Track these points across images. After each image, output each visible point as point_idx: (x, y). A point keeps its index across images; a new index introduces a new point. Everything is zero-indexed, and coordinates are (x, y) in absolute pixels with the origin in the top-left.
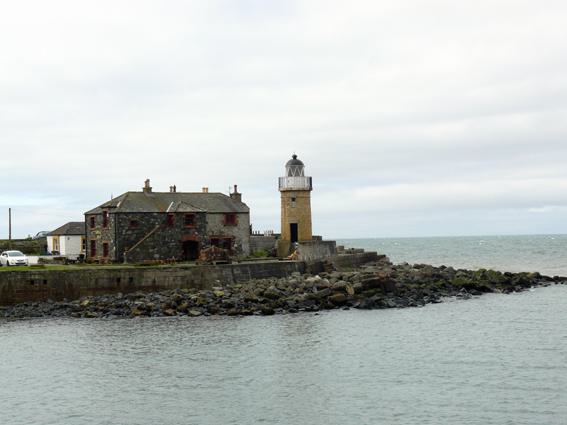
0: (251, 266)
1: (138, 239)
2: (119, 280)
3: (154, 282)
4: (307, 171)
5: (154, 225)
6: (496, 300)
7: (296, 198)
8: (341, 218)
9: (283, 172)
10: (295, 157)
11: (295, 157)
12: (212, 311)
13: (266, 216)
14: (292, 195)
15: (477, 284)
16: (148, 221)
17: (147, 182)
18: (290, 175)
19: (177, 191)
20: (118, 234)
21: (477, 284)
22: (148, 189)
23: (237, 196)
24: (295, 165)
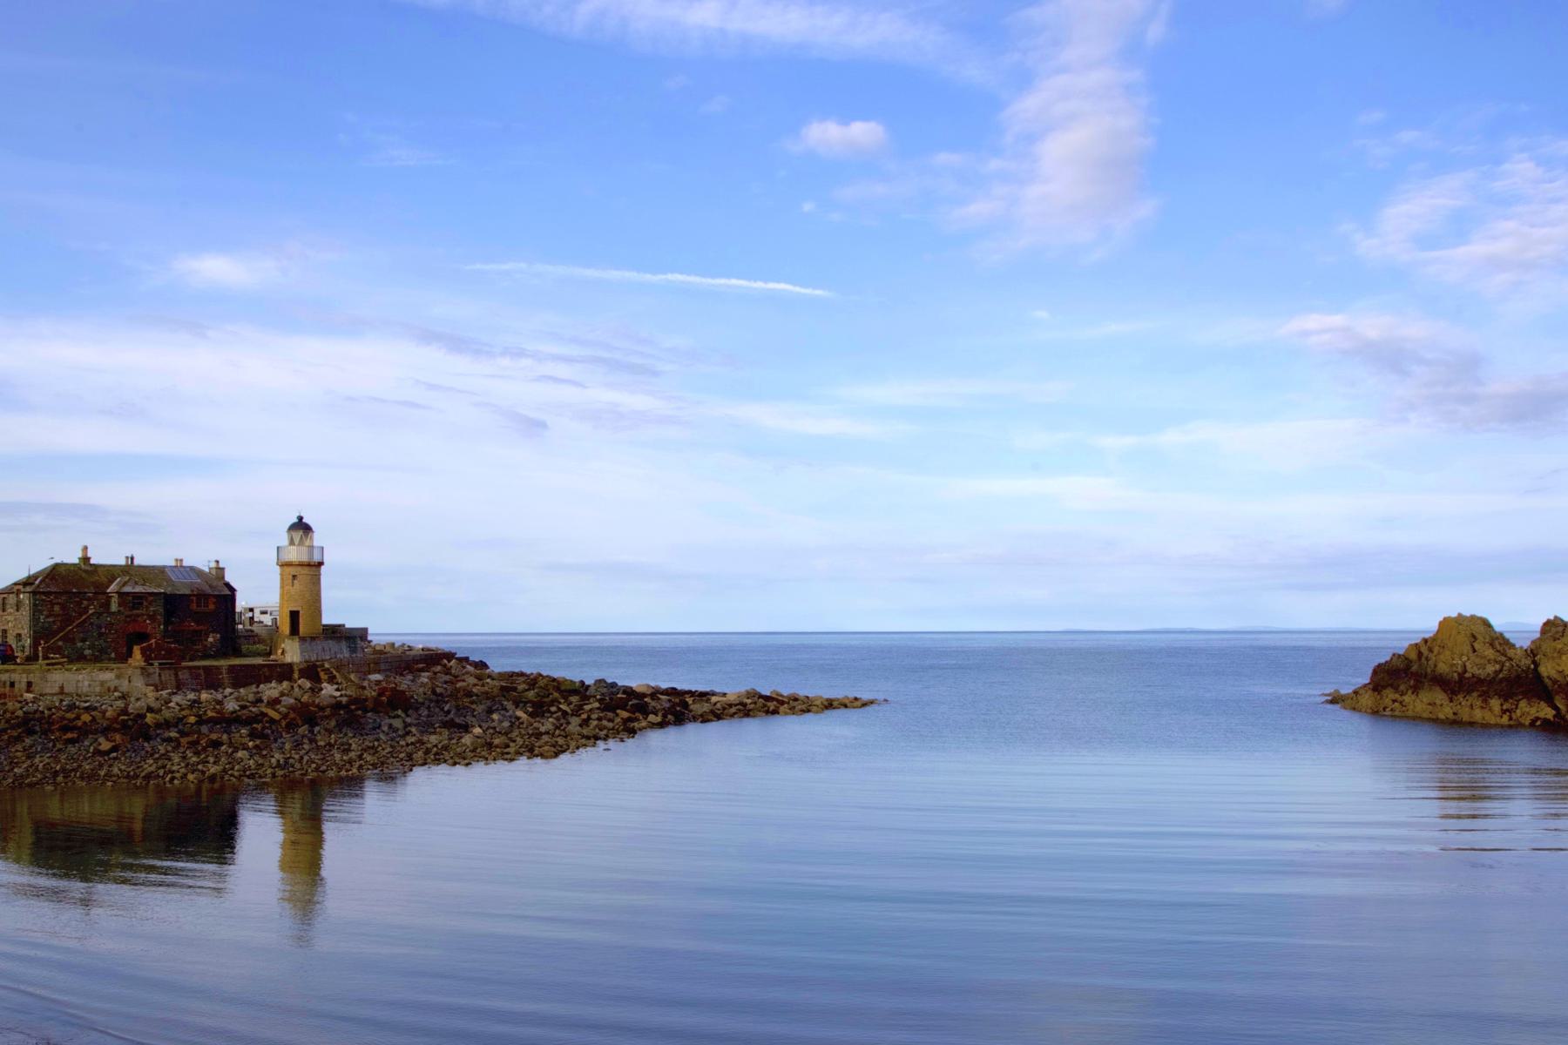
0: (205, 668)
1: (61, 629)
2: (12, 685)
3: (62, 688)
4: (318, 539)
5: (86, 609)
6: (788, 728)
7: (305, 573)
8: (389, 598)
9: (285, 541)
10: (301, 518)
11: (301, 518)
12: (719, 717)
13: (259, 593)
14: (293, 570)
15: (678, 709)
16: (79, 604)
17: (85, 548)
18: (292, 543)
19: (136, 562)
20: (34, 619)
21: (678, 709)
22: (86, 559)
23: (220, 571)
24: (301, 527)
